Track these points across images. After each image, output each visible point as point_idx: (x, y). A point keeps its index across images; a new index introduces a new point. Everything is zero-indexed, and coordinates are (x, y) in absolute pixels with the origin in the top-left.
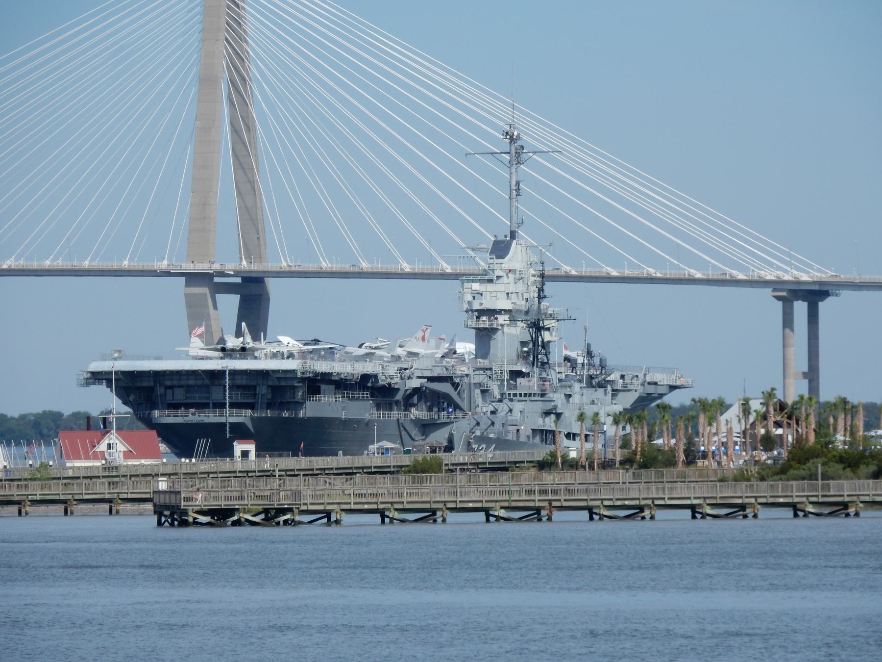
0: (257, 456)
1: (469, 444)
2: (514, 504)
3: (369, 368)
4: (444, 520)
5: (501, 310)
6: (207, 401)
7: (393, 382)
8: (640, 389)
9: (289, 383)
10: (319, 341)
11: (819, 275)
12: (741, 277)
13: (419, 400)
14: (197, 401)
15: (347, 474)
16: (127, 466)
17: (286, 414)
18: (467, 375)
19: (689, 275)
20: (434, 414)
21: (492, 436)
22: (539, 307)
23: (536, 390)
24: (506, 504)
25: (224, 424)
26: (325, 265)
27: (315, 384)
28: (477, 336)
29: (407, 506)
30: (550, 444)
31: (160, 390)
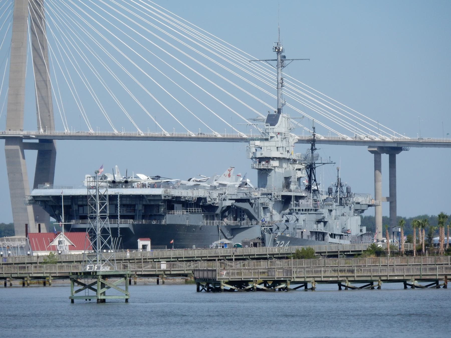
0: (152, 248)
1: (275, 241)
2: (423, 277)
3: (201, 193)
4: (379, 288)
7: (215, 202)
9: (156, 203)
10: (160, 177)
11: (396, 137)
12: (349, 139)
13: (229, 214)
16: (71, 255)
17: (154, 222)
18: (258, 198)
20: (237, 223)
21: (288, 235)
22: (312, 156)
23: (311, 207)
24: (418, 277)
26: (92, 131)
27: (172, 203)
28: (259, 173)
29: (357, 279)
30: (321, 241)
31: (75, 207)
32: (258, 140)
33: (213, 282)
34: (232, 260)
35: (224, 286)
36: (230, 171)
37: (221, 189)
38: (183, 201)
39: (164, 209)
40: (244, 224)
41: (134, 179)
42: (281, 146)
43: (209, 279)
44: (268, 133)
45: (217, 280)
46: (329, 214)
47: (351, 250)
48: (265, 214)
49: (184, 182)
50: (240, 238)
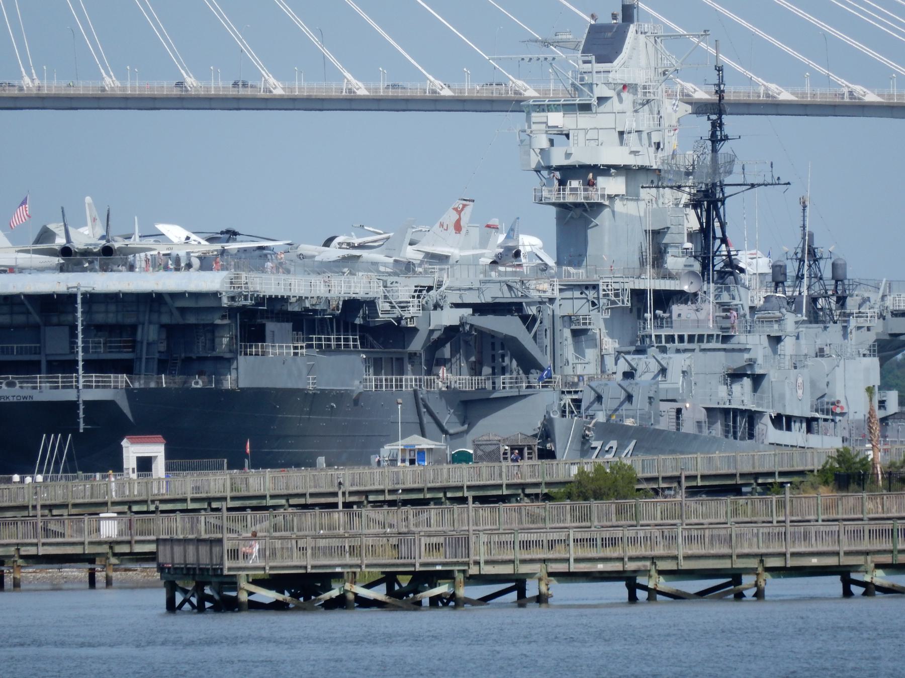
0: (168, 468)
1: (585, 439)
3: (358, 286)
5: (609, 167)
6: (35, 358)
7: (406, 315)
8: (878, 327)
9: (206, 319)
10: (235, 233)
14: (16, 357)
15: (254, 509)
17: (198, 383)
18: (552, 300)
19: (768, 96)
21: (629, 422)
22: (714, 160)
24: (886, 559)
25: (73, 405)
26: (111, 83)
27: (257, 319)
28: (560, 218)
29: (685, 565)
30: (742, 439)
32: (556, 108)
33: (214, 580)
34: (334, 506)
35: (250, 593)
36: (459, 212)
37: (426, 271)
38: (294, 314)
39: (231, 338)
40: (505, 385)
41: (135, 242)
42: (634, 127)
43: (201, 569)
44: (590, 86)
45: (226, 572)
46: (769, 350)
47: (778, 469)
48: (579, 351)
49: (306, 249)
50: (499, 427)
